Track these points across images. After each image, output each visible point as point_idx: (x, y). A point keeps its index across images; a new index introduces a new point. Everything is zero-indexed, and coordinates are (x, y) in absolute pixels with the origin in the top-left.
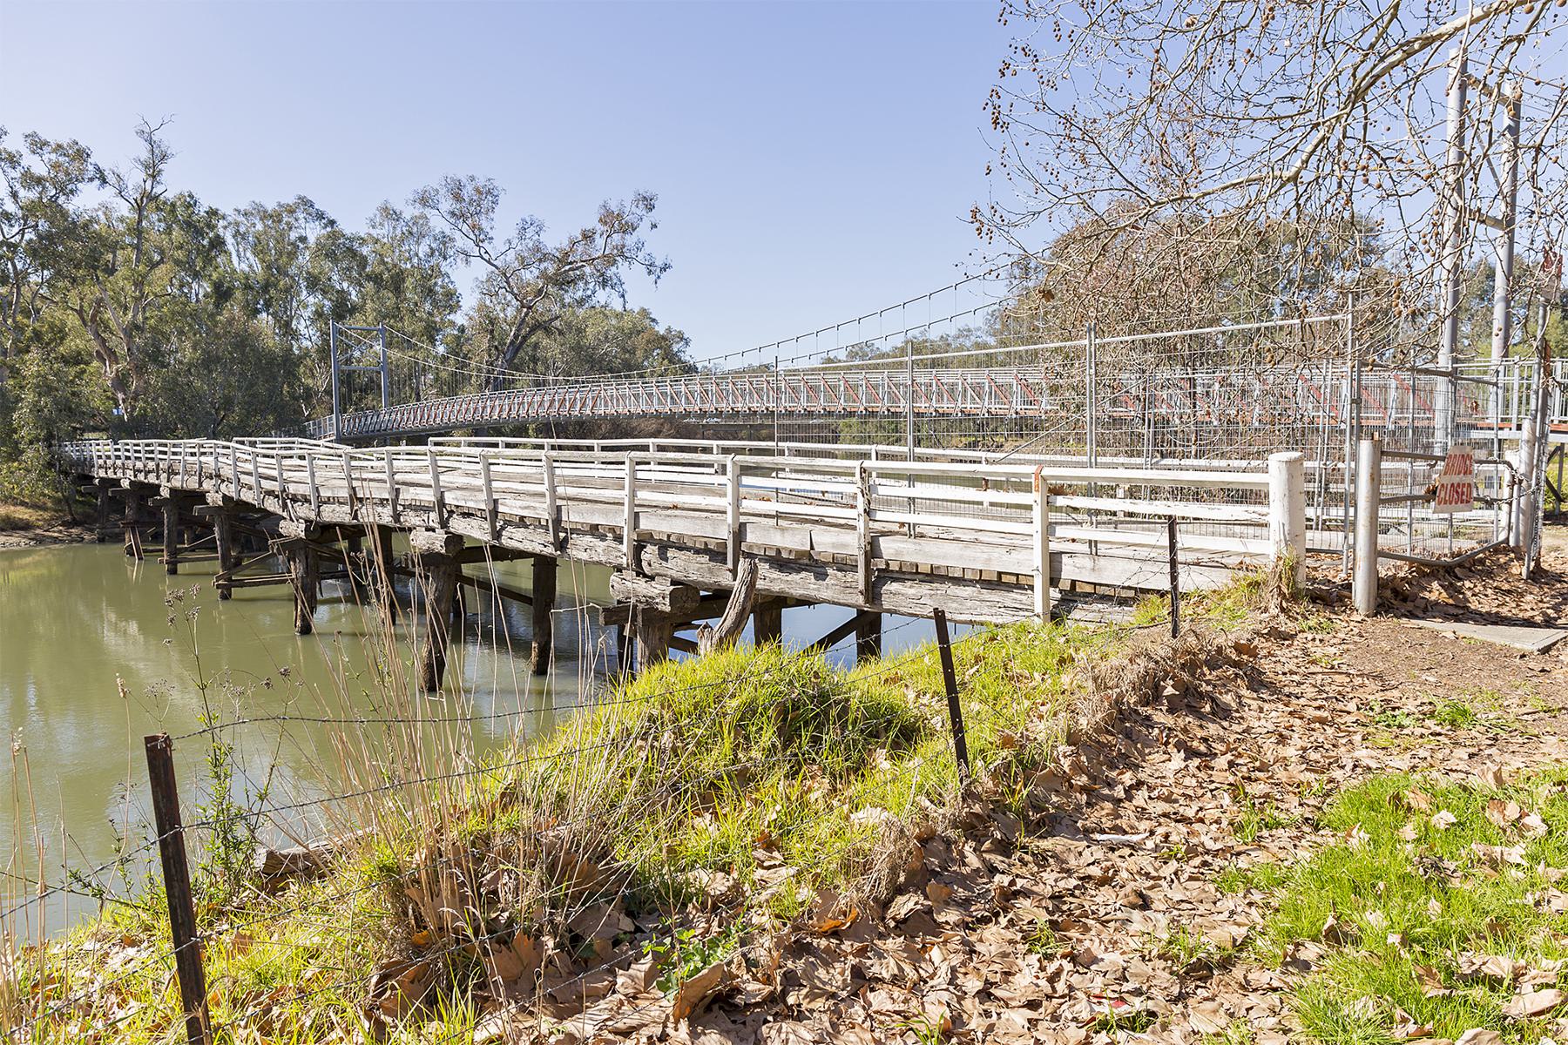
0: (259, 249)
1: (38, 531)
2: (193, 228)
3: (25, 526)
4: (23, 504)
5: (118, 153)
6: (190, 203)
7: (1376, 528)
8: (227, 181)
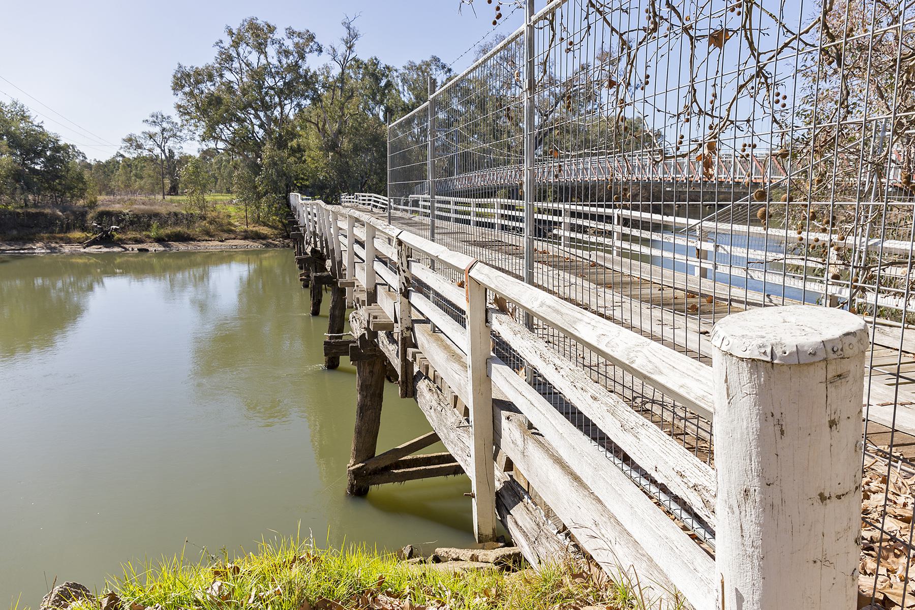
0: (412, 89)
1: (270, 241)
4: (268, 226)
5: (330, 36)
7: (887, 202)
8: (397, 55)
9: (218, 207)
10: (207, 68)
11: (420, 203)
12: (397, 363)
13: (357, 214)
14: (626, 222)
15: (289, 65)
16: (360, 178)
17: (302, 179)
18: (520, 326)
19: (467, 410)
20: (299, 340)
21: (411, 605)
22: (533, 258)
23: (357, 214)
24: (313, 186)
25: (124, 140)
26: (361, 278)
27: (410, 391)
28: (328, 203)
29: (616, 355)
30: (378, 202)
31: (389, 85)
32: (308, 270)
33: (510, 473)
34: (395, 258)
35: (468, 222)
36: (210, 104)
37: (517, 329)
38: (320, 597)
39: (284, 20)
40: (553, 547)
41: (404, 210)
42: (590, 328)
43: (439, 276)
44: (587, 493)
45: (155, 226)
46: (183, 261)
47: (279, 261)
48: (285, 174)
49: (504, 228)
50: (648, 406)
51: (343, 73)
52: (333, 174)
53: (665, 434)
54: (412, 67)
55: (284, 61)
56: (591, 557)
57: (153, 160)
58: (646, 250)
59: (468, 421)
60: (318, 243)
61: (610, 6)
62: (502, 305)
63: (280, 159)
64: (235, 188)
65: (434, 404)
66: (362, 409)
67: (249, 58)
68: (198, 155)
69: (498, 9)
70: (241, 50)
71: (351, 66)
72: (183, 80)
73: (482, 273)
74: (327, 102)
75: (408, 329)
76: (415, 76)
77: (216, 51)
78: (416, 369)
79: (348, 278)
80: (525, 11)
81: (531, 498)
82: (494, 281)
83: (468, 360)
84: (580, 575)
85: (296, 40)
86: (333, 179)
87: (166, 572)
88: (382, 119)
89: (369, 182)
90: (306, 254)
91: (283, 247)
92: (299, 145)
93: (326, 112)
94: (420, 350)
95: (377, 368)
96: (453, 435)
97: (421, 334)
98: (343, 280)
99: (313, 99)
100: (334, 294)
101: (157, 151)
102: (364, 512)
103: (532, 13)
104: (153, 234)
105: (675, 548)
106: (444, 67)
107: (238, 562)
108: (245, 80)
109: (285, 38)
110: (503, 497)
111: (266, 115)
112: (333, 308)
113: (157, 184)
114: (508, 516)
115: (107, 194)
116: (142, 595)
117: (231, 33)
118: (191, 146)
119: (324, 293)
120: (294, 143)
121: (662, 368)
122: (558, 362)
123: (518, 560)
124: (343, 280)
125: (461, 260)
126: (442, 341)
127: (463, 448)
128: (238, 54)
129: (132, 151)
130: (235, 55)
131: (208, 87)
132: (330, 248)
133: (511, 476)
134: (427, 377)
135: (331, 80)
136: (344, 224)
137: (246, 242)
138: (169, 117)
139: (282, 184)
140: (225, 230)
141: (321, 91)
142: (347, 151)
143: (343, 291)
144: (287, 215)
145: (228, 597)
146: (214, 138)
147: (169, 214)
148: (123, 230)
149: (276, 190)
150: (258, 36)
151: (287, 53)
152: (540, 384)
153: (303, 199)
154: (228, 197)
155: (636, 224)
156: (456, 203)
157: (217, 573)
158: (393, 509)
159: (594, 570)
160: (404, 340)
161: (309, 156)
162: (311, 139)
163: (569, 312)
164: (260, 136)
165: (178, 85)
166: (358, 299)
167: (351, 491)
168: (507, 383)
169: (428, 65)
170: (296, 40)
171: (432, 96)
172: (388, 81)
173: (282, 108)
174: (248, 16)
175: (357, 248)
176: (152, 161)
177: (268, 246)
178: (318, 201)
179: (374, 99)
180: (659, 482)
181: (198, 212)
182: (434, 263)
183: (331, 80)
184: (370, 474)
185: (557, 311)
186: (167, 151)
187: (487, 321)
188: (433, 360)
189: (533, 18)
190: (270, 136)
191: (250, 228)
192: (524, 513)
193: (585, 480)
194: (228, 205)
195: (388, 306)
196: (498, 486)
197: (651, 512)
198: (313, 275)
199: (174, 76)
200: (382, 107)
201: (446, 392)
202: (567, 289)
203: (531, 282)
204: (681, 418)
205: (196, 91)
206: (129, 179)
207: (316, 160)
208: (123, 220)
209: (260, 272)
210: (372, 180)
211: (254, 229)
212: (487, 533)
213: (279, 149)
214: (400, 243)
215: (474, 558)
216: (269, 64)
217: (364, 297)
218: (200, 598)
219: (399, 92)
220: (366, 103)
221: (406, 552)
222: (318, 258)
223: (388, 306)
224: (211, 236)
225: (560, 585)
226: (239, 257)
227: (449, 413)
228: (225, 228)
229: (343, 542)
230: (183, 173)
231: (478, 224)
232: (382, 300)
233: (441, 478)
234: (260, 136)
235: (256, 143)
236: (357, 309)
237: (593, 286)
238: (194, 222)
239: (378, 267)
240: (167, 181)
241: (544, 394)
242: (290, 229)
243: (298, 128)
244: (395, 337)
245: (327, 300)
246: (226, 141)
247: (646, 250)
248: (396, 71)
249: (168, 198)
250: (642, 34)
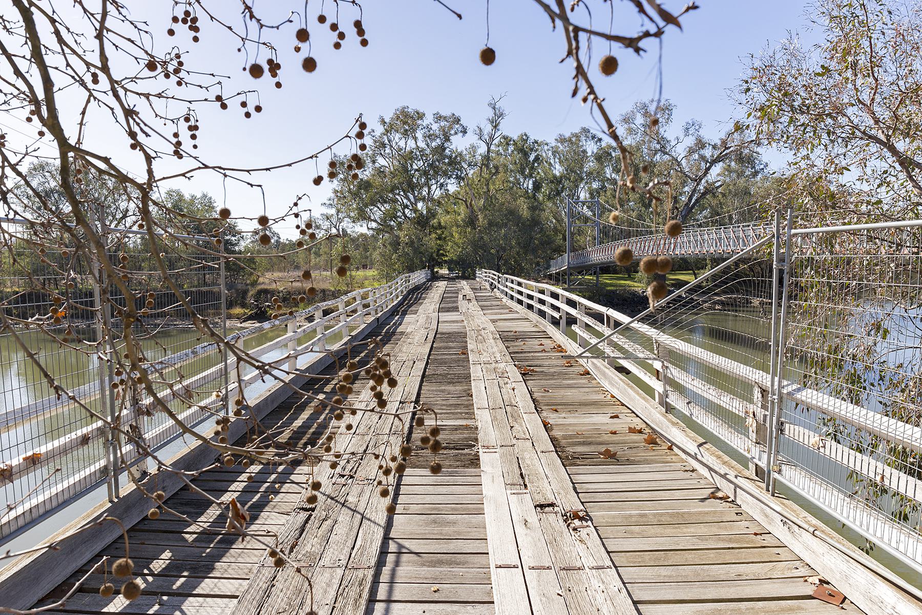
6: (524, 138)
39: (430, 105)
106: (594, 137)
115: (280, 271)
117: (383, 122)
130: (387, 142)
169: (577, 136)
170: (442, 124)
173: (429, 188)
174: (399, 105)
179: (523, 173)
248: (547, 144)
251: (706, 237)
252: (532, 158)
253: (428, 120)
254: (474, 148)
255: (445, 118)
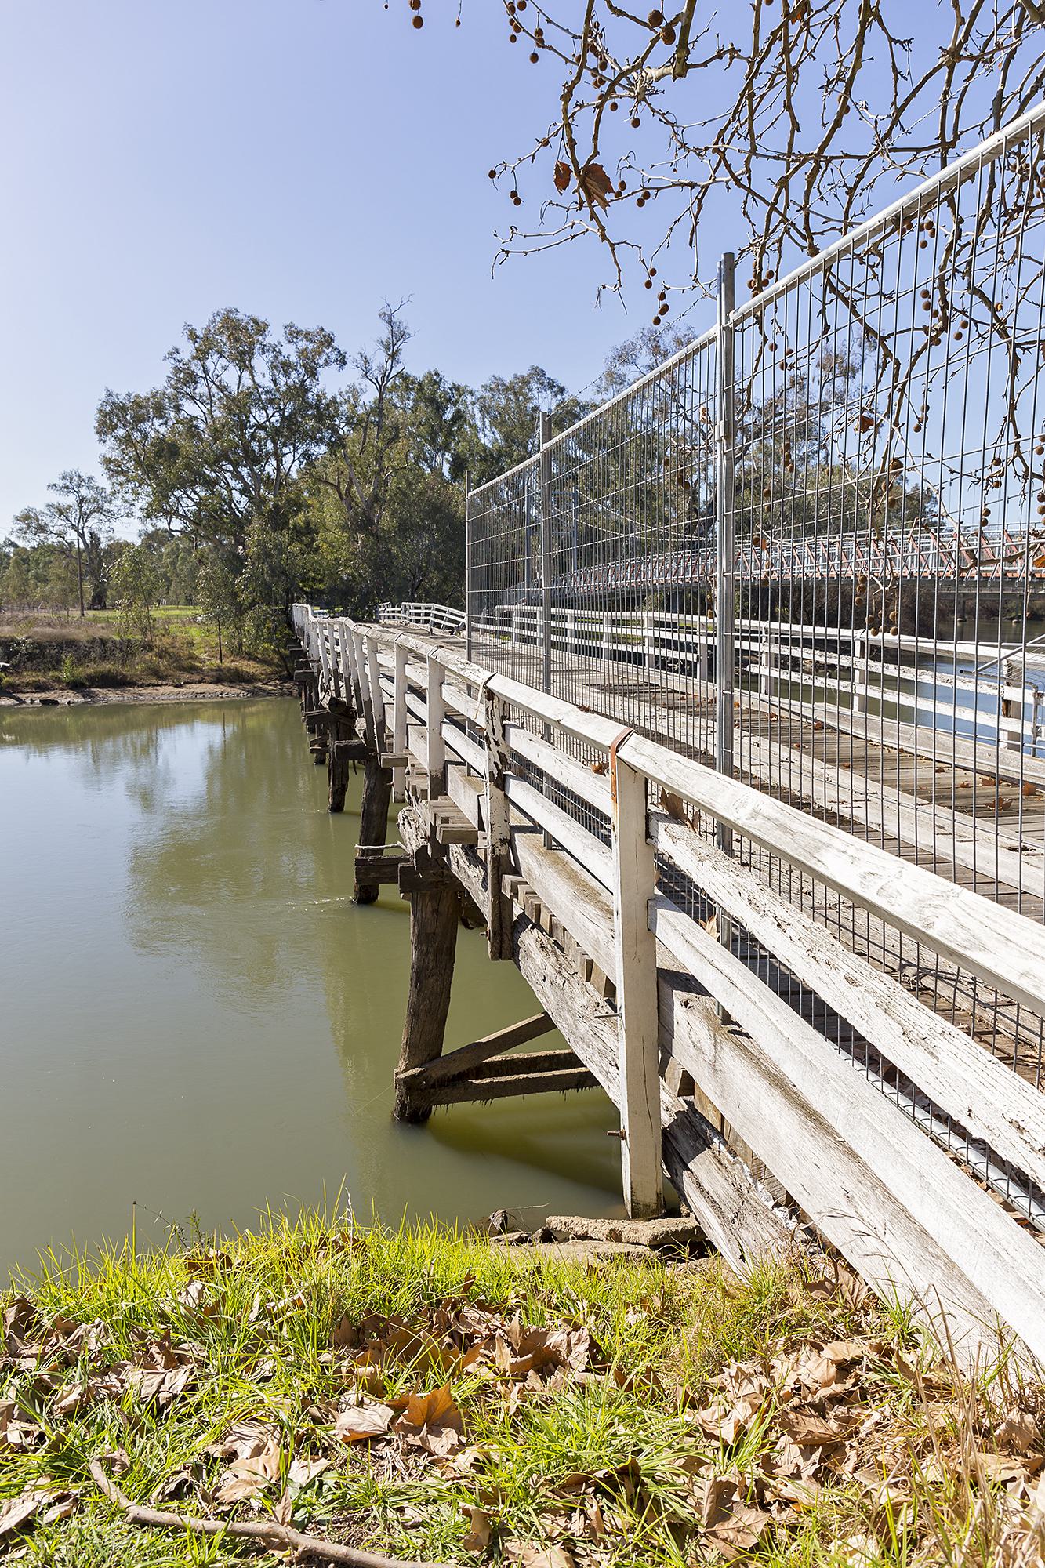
0: (498, 423)
1: (259, 684)
2: (437, 406)
3: (249, 679)
4: (255, 659)
5: (361, 338)
6: (435, 380)
8: (468, 362)
9: (172, 628)
10: (154, 396)
11: (516, 619)
12: (483, 900)
13: (412, 642)
14: (874, 652)
15: (289, 388)
16: (410, 577)
17: (314, 579)
18: (709, 846)
19: (610, 990)
20: (312, 857)
21: (522, 1327)
22: (731, 721)
23: (412, 642)
24: (331, 591)
25: (17, 519)
26: (420, 752)
27: (506, 947)
28: (356, 620)
29: (898, 911)
30: (442, 618)
31: (459, 417)
32: (323, 734)
33: (688, 1098)
34: (481, 721)
35: (596, 652)
36: (159, 455)
37: (704, 852)
38: (368, 1312)
39: (281, 309)
40: (768, 1232)
41: (487, 631)
42: (845, 860)
43: (560, 754)
44: (831, 1142)
45: (68, 662)
46: (115, 721)
47: (273, 717)
48: (284, 573)
49: (660, 663)
50: (928, 981)
51: (381, 399)
52: (365, 570)
53: (961, 1033)
54: (498, 386)
55: (282, 380)
56: (839, 1253)
57: (65, 550)
58: (907, 700)
59: (614, 1008)
60: (343, 690)
61: (862, 289)
62: (675, 808)
63: (276, 546)
64: (200, 597)
65: (550, 972)
66: (421, 975)
67: (223, 377)
68: (138, 542)
69: (662, 296)
70: (209, 364)
71: (395, 387)
72: (115, 416)
73: (641, 753)
74: (354, 448)
75: (503, 841)
76: (503, 402)
77: (168, 367)
78: (517, 911)
79: (396, 752)
80: (718, 305)
81: (725, 1143)
82: (665, 768)
83: (616, 903)
84: (820, 1286)
85: (302, 344)
86: (365, 579)
87: (111, 1266)
88: (447, 474)
89: (426, 584)
90: (323, 708)
91: (282, 695)
92: (307, 523)
93: (352, 465)
94: (525, 877)
95: (445, 906)
96: (583, 1028)
97: (526, 849)
98: (389, 755)
99: (331, 446)
100: (369, 776)
101: (72, 535)
102: (425, 1156)
103: (730, 306)
104: (65, 676)
105: (1003, 1253)
106: (551, 384)
107: (227, 1246)
108: (217, 414)
109: (284, 341)
110: (675, 1138)
111: (252, 473)
112: (369, 800)
113: (72, 591)
114: (685, 1173)
116: (72, 1302)
117: (193, 336)
118: (127, 527)
119: (351, 773)
120: (299, 519)
121: (984, 939)
122: (781, 913)
123: (699, 1245)
124: (389, 755)
125: (605, 732)
126: (564, 864)
127: (605, 1051)
128: (206, 371)
129: (29, 536)
130: (200, 373)
131: (156, 428)
132: (364, 698)
133: (690, 1104)
134: (537, 925)
135: (361, 411)
136: (388, 660)
137: (219, 688)
138: (90, 479)
139: (279, 590)
140: (185, 668)
141: (344, 429)
142: (389, 531)
143: (386, 774)
144: (288, 642)
145: (214, 1309)
146: (166, 513)
147: (93, 641)
148: (16, 669)
149: (269, 599)
150: (238, 340)
151: (287, 367)
152: (735, 940)
153: (315, 615)
154: (189, 612)
155: (890, 655)
156: (576, 620)
157: (193, 1267)
158: (472, 1145)
159: (845, 1276)
160: (496, 860)
161: (325, 541)
162: (329, 512)
163: (807, 830)
164: (241, 507)
165: (105, 426)
166: (414, 788)
167: (402, 1115)
168: (682, 941)
169: (525, 382)
170: (302, 344)
171: (546, 445)
172: (458, 411)
173: (279, 461)
174: (221, 306)
175: (411, 700)
176: (63, 552)
177: (254, 693)
178: (341, 619)
179: (433, 442)
180: (975, 1136)
181: (139, 637)
182: (549, 731)
183: (361, 411)
184: (433, 1086)
185: (784, 828)
186: (87, 536)
187: (648, 835)
188: (549, 896)
189: (733, 316)
190: (259, 508)
191: (226, 663)
192: (713, 1168)
193: (831, 1122)
194: (187, 624)
195: (467, 801)
196: (667, 1119)
197: (957, 1185)
198: (332, 744)
199: (100, 411)
200: (448, 456)
201: (571, 953)
202: (775, 770)
203: (730, 770)
204: (986, 1006)
205: (136, 435)
206: (26, 583)
207: (337, 546)
208: (17, 652)
209: (243, 737)
210: (431, 579)
211: (233, 665)
212: (647, 1201)
213: (274, 530)
214: (490, 695)
215: (615, 1236)
216: (257, 386)
217: (425, 784)
218: (168, 1310)
219: (476, 429)
220: (421, 449)
221: (497, 1222)
222: (342, 715)
223: (467, 801)
224: (161, 678)
225: (784, 1303)
226: (209, 713)
227: (577, 988)
228: (185, 664)
229: (399, 1212)
230: (114, 572)
231: (616, 656)
232: (455, 791)
233: (554, 1095)
234: (241, 507)
235: (236, 521)
236: (411, 803)
237: (819, 764)
238: (133, 655)
239: (450, 733)
240: (87, 586)
241: (743, 958)
242: (293, 666)
243: (306, 494)
244: (481, 854)
245: (358, 785)
246: (185, 517)
247: (907, 700)
248: (471, 393)
249: (91, 613)
250: (922, 338)
251: (837, 549)
252: (449, 414)
253: (275, 335)
254: (354, 391)
255: (308, 336)
